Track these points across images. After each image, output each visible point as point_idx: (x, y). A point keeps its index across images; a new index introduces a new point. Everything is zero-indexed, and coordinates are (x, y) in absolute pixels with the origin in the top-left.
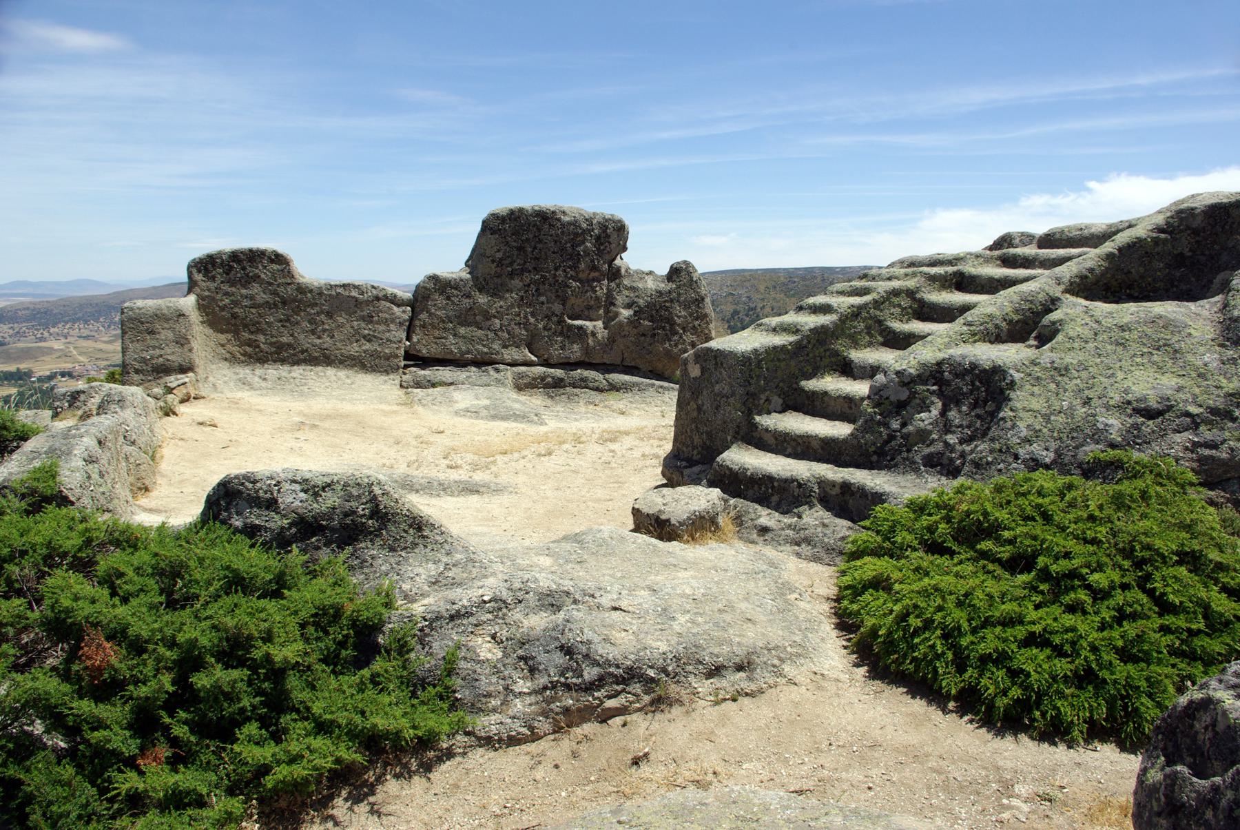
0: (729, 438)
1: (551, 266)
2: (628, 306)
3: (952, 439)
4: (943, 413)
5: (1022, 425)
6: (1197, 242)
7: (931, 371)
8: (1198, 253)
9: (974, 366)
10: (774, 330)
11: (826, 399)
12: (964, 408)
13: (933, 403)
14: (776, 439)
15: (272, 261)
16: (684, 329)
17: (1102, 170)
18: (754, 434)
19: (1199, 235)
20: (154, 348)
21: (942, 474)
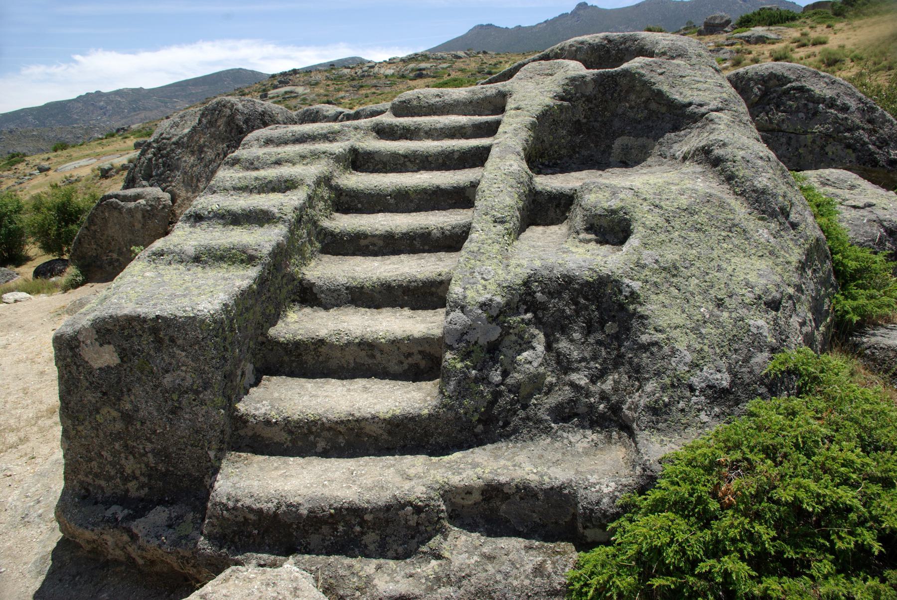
0: (212, 454)
4: (549, 347)
5: (681, 346)
6: (590, 109)
7: (521, 295)
8: (592, 119)
10: (197, 259)
11: (323, 350)
12: (576, 336)
13: (533, 336)
14: (290, 432)
17: (86, 46)
18: (242, 433)
19: (591, 102)
21: (584, 428)
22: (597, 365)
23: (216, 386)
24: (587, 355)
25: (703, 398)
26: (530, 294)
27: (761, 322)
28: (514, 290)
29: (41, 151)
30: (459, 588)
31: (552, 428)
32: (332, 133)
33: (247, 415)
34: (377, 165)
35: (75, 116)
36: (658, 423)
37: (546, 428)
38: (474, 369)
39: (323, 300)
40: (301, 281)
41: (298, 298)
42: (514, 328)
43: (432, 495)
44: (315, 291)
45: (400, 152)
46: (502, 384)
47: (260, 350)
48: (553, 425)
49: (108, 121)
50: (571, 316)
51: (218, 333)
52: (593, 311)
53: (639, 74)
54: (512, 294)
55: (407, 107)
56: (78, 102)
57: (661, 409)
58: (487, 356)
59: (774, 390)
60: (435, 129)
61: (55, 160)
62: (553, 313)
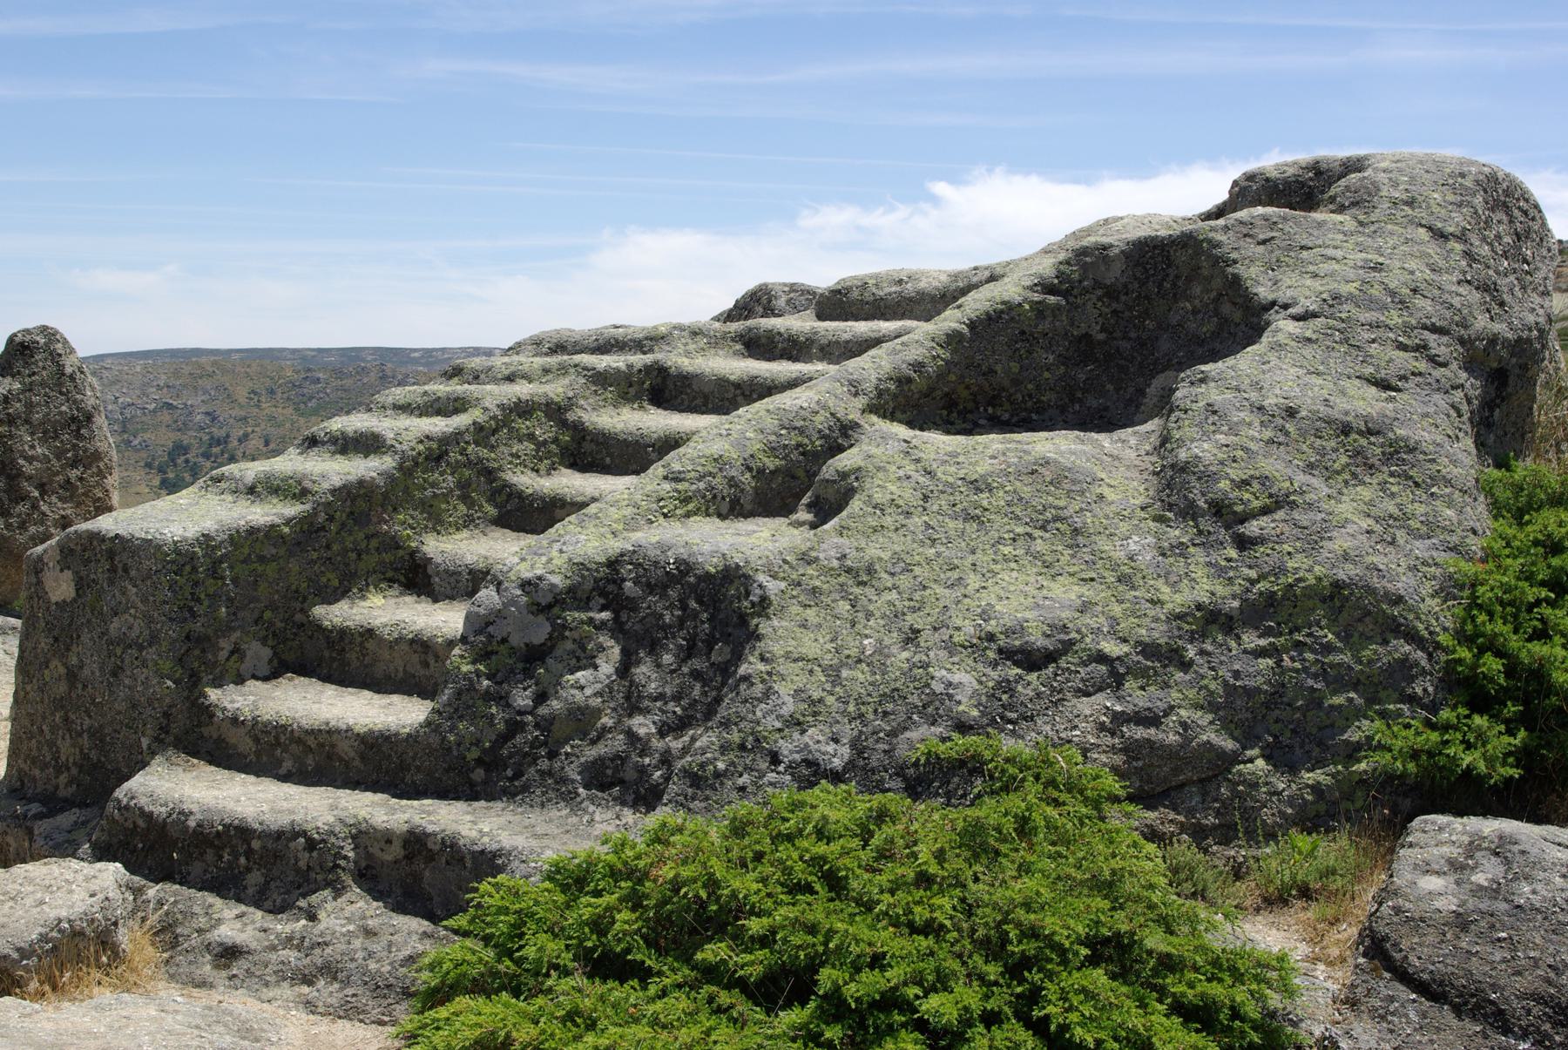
0: (145, 742)
3: (643, 725)
4: (624, 670)
6: (1115, 312)
7: (596, 581)
8: (1118, 334)
10: (251, 490)
11: (370, 645)
12: (667, 658)
13: (601, 648)
14: (257, 740)
16: (42, 488)
19: (1117, 300)
21: (623, 804)
22: (677, 709)
23: (164, 644)
24: (668, 690)
25: (789, 777)
26: (614, 582)
27: (958, 677)
28: (588, 570)
30: (307, 956)
31: (578, 795)
32: (651, 339)
33: (217, 706)
34: (695, 398)
36: (693, 799)
37: (570, 792)
38: (488, 679)
39: (437, 588)
40: (413, 553)
41: (402, 579)
42: (571, 630)
43: (337, 829)
44: (430, 570)
45: (732, 378)
46: (530, 713)
47: (295, 634)
48: (581, 790)
50: (670, 626)
51: (182, 570)
52: (703, 622)
53: (1209, 241)
54: (583, 576)
55: (841, 300)
57: (707, 779)
58: (520, 666)
59: (920, 789)
60: (837, 342)
62: (644, 618)
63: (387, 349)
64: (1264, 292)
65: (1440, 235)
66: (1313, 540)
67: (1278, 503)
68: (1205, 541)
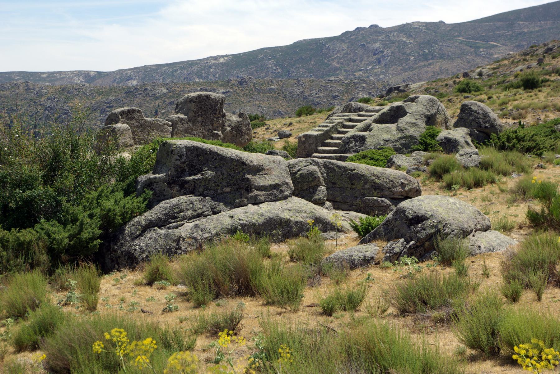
1: (209, 113)
2: (229, 126)
3: (357, 147)
9: (359, 135)
10: (317, 131)
15: (138, 112)
16: (245, 134)
20: (124, 139)
29: (281, 115)
35: (335, 64)
49: (382, 73)
56: (343, 41)
61: (297, 126)
63: (27, 72)
64: (407, 111)
65: (424, 105)
66: (409, 132)
67: (406, 129)
68: (400, 132)
